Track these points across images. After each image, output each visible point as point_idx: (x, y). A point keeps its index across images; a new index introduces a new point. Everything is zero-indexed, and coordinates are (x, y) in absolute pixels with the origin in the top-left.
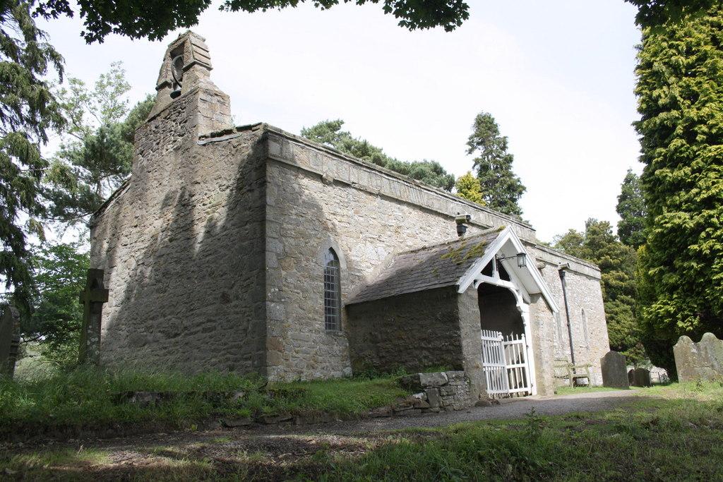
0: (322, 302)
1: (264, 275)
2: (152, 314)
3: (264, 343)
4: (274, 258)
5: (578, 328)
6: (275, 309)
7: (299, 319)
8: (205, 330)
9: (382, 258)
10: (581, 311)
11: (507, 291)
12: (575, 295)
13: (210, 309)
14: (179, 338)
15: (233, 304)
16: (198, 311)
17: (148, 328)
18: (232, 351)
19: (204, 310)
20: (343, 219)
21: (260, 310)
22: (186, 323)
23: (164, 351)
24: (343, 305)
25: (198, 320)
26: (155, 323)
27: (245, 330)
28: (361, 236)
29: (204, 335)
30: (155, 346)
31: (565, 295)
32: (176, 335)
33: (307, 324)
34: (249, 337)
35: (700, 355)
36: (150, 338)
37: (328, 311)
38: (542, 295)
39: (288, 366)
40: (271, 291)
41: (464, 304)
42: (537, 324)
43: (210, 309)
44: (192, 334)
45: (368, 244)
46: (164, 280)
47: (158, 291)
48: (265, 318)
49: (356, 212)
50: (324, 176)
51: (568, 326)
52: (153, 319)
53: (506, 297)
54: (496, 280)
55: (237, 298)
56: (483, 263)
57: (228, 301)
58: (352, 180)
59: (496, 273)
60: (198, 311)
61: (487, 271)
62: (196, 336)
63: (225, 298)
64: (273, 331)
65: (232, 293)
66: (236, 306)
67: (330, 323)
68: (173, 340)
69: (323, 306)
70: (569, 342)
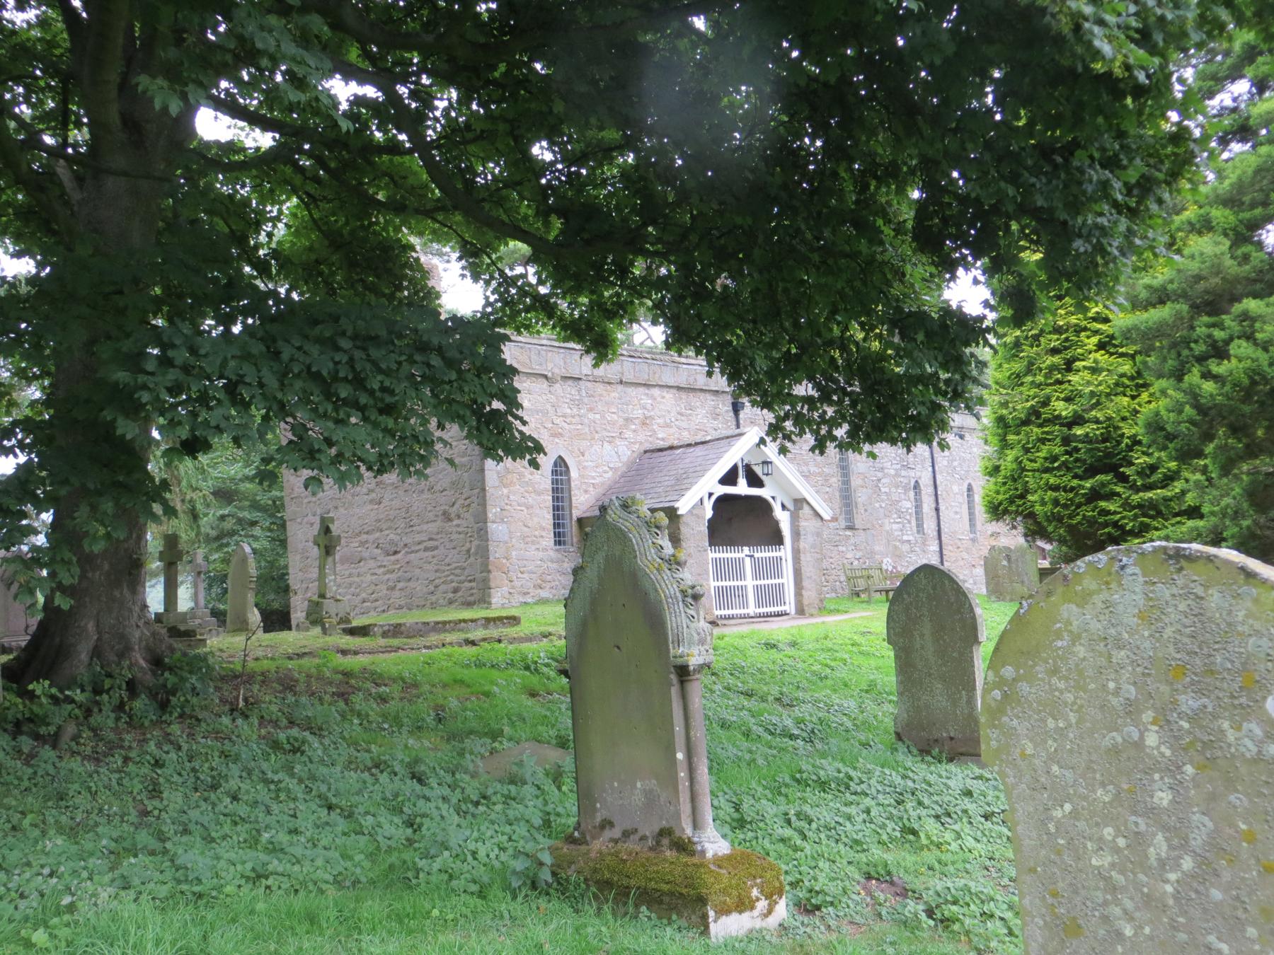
0: (550, 517)
1: (484, 496)
2: (367, 528)
3: (487, 565)
4: (495, 476)
5: (956, 513)
6: (496, 530)
7: (524, 538)
8: (426, 549)
9: (625, 459)
10: (965, 489)
11: (759, 500)
12: (955, 464)
13: (433, 527)
14: (399, 556)
15: (455, 523)
16: (418, 528)
17: (362, 544)
18: (457, 571)
19: (425, 527)
20: (574, 421)
21: (482, 532)
22: (405, 540)
23: (382, 570)
24: (575, 518)
25: (418, 538)
26: (371, 538)
27: (468, 551)
28: (597, 436)
29: (427, 554)
30: (372, 564)
31: (933, 466)
32: (396, 553)
33: (533, 543)
34: (472, 559)
35: (1010, 567)
36: (366, 554)
37: (556, 525)
38: (805, 500)
39: (513, 587)
40: (492, 512)
41: (687, 525)
42: (796, 534)
43: (433, 527)
44: (412, 552)
45: (606, 444)
46: (378, 490)
47: (371, 501)
48: (487, 540)
49: (591, 410)
50: (550, 375)
51: (937, 510)
52: (367, 533)
53: (760, 508)
54: (742, 488)
55: (459, 517)
56: (722, 468)
57: (450, 520)
58: (585, 372)
59: (742, 481)
60: (418, 528)
61: (730, 478)
62: (418, 555)
63: (447, 517)
64: (496, 552)
65: (453, 511)
66: (458, 526)
67: (559, 539)
68: (393, 558)
69: (552, 522)
70: (936, 533)
